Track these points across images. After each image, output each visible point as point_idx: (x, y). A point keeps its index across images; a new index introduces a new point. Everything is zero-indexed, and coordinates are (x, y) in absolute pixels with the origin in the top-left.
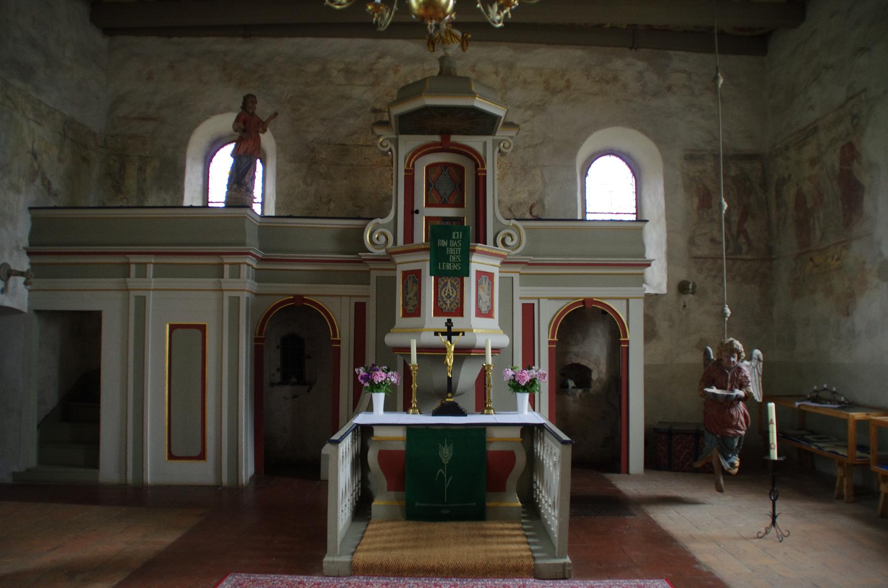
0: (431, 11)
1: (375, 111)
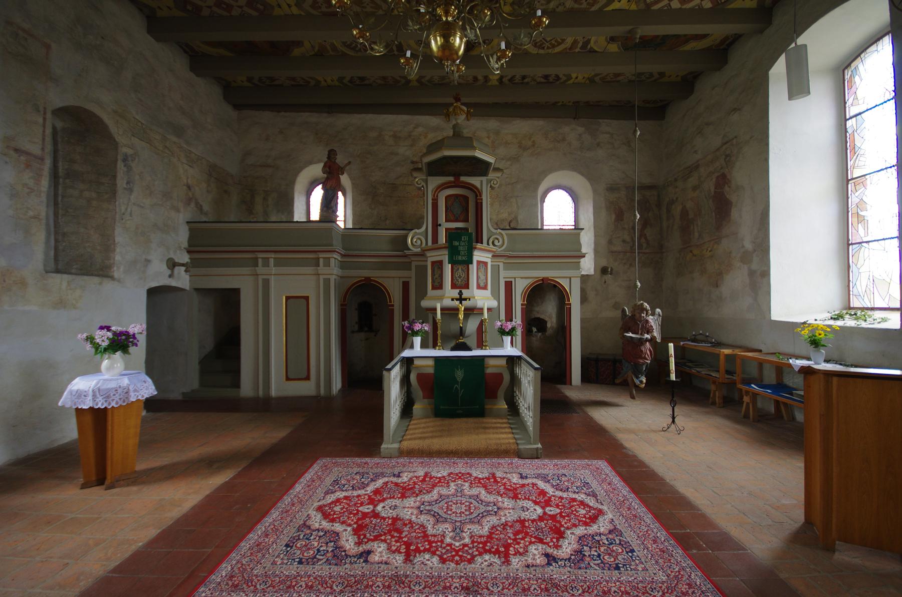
0: (447, 53)
1: (413, 162)
